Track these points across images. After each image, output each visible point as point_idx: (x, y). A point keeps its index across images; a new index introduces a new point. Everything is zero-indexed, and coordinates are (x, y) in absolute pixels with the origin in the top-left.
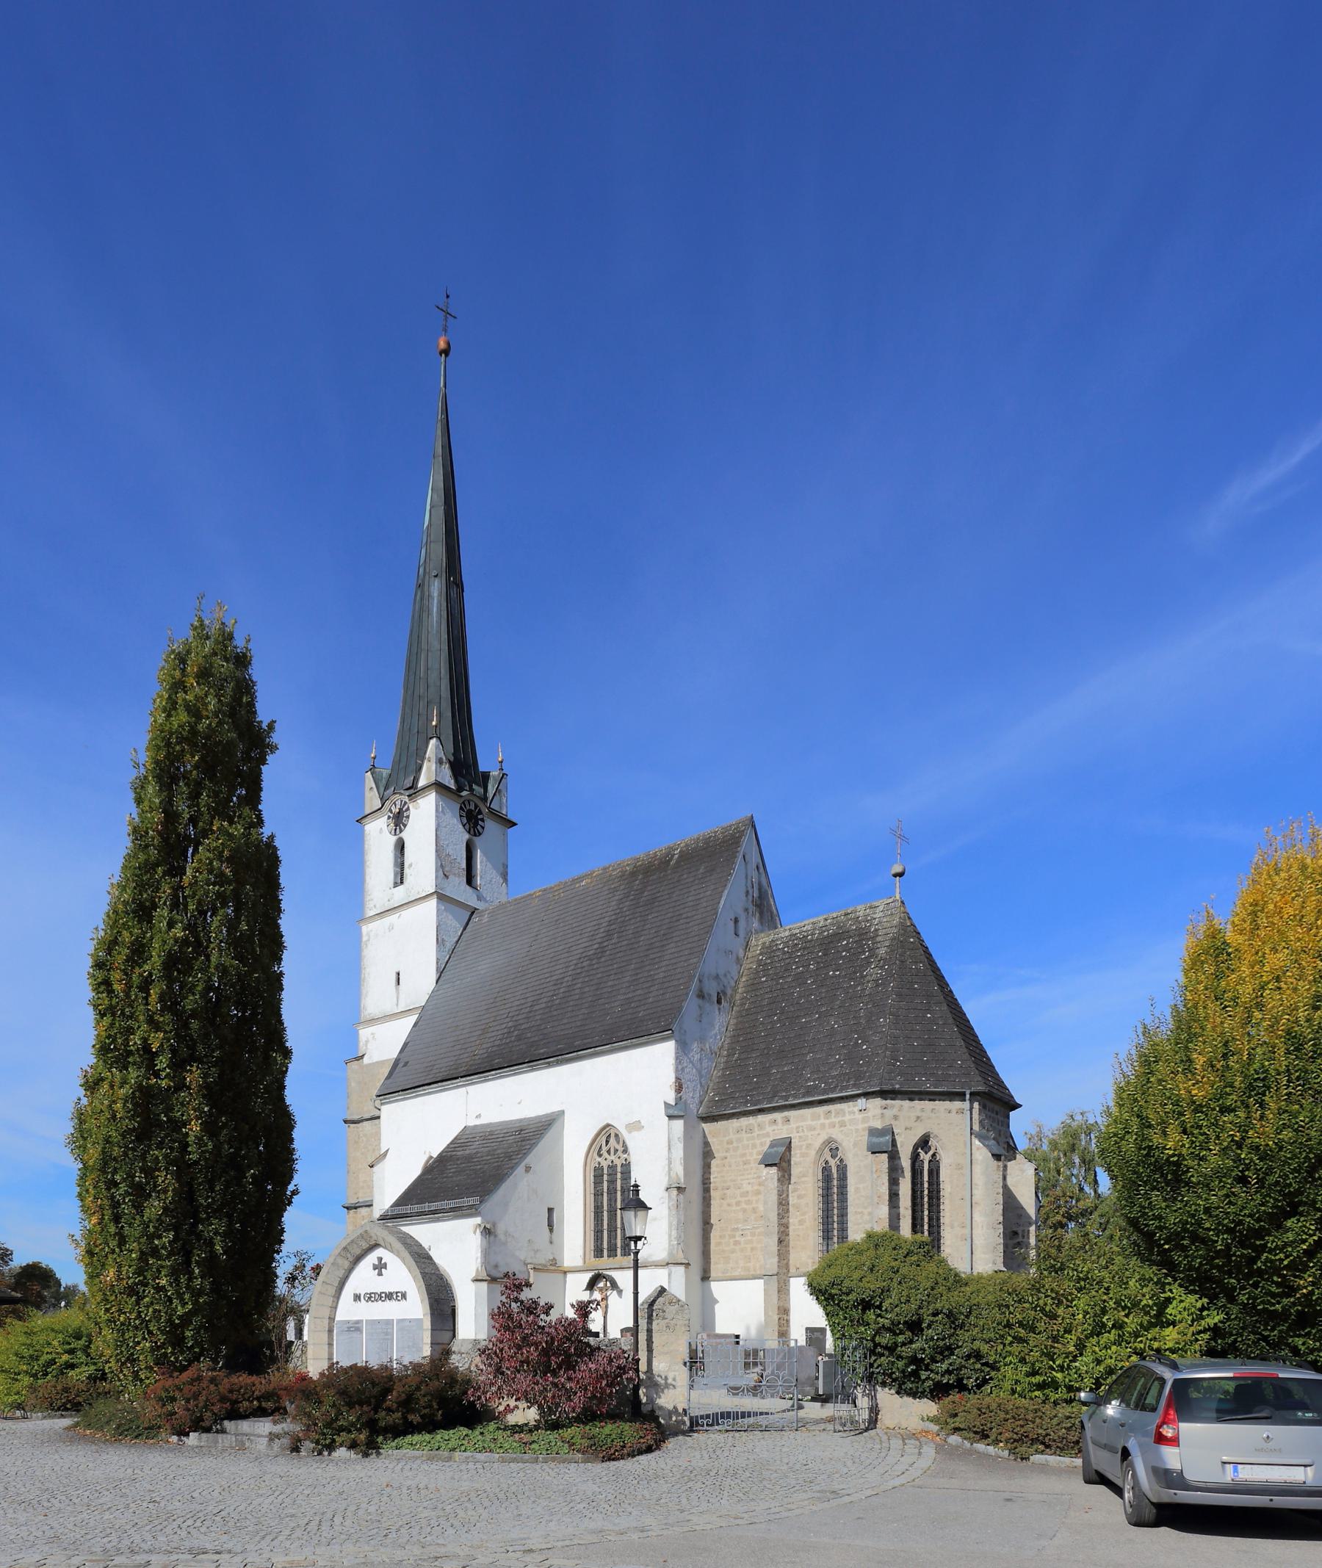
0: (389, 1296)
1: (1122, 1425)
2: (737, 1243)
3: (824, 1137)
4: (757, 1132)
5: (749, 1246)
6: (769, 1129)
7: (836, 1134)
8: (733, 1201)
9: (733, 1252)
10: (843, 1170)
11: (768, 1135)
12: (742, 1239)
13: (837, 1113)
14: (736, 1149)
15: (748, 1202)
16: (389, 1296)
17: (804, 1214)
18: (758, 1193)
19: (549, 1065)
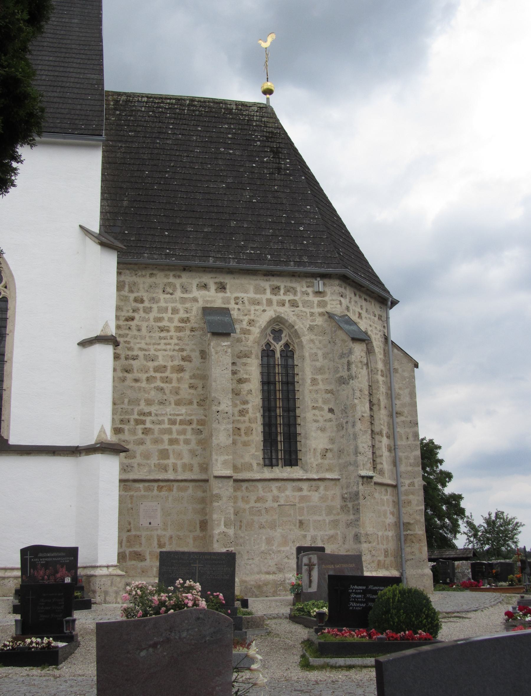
0: (126, 264)
1: (153, 360)
2: (146, 431)
3: (270, 314)
4: (179, 294)
5: (166, 437)
6: (196, 293)
7: (287, 312)
8: (144, 376)
9: (142, 442)
10: (288, 353)
11: (195, 300)
12: (156, 428)
13: (287, 291)
14: (148, 310)
15: (166, 380)
16: (126, 264)
17: (246, 402)
18: (181, 369)
19: (485, 592)
